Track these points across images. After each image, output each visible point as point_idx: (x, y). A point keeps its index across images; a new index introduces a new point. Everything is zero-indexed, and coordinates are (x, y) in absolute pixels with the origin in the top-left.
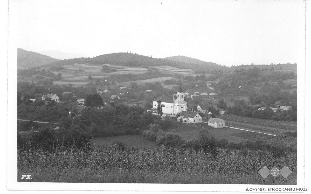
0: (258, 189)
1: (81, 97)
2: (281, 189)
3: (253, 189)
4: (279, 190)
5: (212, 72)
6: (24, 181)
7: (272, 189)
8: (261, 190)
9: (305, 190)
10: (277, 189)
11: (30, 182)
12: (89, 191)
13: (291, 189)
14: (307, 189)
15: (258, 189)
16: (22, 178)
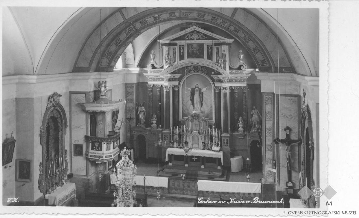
0: (298, 212)
1: (203, 169)
2: (325, 212)
3: (292, 213)
4: (322, 213)
5: (294, 163)
6: (11, 204)
7: (314, 212)
8: (301, 213)
9: (352, 213)
10: (320, 213)
11: (265, 207)
12: (111, 214)
13: (336, 212)
14: (355, 212)
15: (298, 212)
16: (8, 201)
